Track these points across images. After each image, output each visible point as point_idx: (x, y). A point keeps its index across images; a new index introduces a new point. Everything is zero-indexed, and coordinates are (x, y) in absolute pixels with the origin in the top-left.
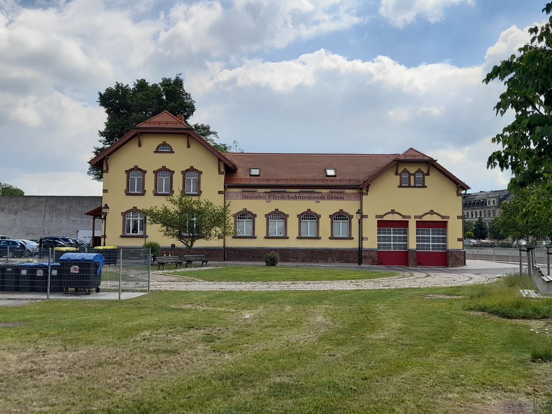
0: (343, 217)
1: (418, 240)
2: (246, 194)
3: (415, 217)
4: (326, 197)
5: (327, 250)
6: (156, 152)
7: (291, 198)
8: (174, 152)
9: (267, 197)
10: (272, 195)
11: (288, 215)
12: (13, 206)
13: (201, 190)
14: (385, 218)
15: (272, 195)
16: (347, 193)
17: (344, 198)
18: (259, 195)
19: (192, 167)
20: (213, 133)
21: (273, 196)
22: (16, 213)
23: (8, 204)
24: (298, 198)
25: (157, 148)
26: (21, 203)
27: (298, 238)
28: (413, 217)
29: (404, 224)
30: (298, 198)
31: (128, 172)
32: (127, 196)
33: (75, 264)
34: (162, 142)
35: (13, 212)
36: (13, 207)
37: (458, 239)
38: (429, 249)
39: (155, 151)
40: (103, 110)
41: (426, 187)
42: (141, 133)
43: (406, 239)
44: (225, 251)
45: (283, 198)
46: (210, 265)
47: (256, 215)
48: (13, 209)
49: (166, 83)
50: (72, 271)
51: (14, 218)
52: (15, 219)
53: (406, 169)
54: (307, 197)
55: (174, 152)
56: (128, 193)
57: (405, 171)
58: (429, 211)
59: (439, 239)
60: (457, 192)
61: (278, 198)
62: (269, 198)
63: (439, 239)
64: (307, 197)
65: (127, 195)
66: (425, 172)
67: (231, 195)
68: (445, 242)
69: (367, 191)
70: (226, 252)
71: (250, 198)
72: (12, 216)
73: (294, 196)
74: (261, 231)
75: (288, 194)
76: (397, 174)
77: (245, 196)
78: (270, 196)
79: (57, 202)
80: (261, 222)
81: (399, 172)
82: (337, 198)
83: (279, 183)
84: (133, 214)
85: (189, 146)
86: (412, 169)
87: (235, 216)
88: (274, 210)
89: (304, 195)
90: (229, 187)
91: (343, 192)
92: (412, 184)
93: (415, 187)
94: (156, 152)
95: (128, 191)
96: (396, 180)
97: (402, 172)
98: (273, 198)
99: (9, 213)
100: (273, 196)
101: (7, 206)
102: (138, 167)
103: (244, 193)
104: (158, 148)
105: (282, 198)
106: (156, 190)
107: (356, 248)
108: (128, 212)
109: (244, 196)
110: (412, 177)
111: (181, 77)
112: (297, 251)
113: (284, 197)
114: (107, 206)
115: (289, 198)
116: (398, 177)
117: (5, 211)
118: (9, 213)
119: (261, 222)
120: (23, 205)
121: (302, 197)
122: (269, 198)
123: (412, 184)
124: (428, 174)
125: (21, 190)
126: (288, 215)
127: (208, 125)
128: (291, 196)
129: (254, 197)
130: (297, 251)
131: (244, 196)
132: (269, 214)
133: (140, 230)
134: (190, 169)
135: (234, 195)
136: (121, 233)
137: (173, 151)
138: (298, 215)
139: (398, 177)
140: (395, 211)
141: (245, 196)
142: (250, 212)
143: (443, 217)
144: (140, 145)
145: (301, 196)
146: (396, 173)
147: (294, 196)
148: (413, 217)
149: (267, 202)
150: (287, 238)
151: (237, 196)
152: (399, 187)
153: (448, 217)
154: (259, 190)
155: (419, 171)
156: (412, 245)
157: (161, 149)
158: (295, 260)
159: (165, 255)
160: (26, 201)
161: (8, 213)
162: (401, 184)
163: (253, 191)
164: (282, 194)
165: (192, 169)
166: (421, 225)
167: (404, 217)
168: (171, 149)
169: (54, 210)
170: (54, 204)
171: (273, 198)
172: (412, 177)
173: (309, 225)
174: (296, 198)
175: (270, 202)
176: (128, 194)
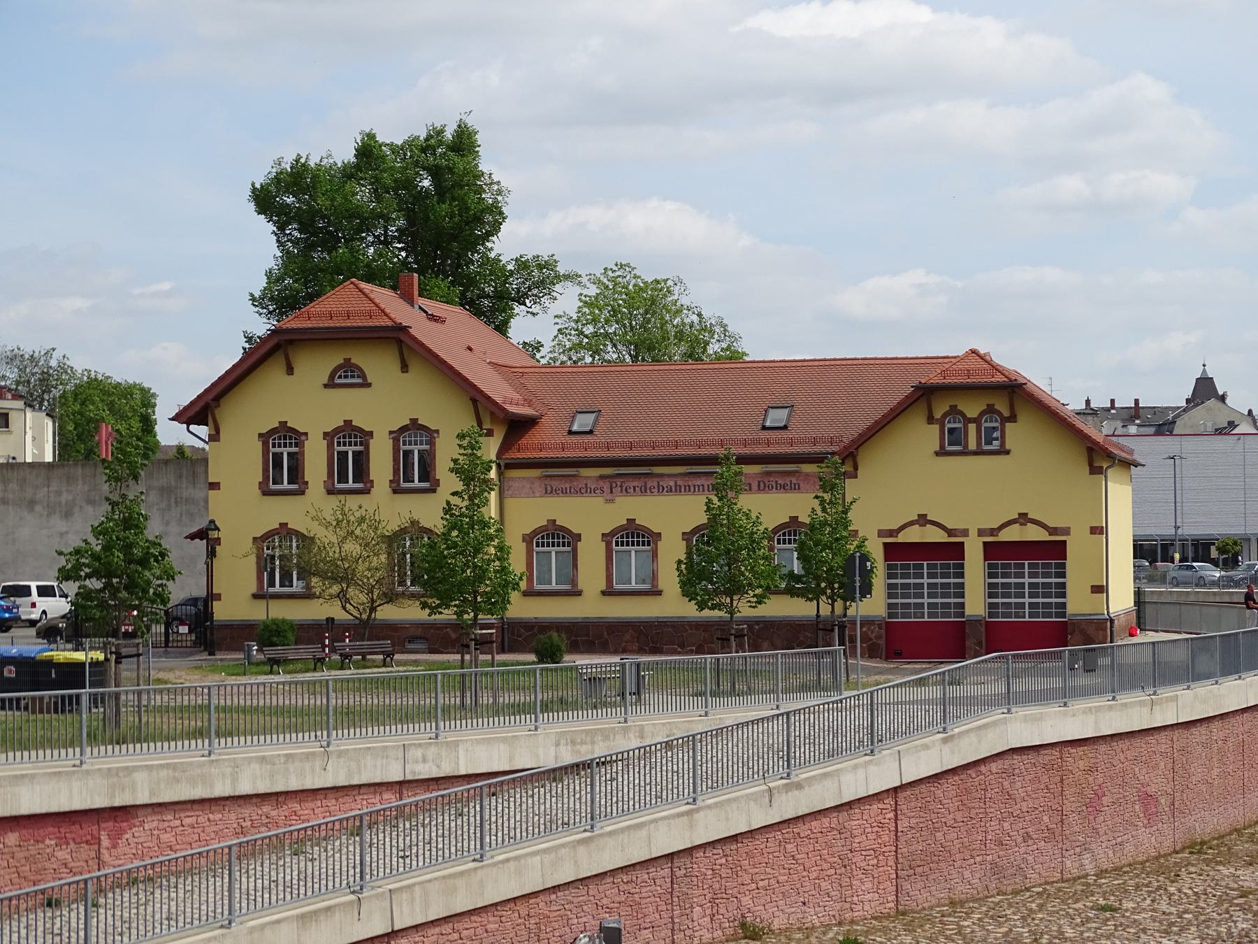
0: (638, 537)
1: (992, 591)
2: (555, 484)
3: (981, 532)
4: (755, 486)
5: (758, 623)
6: (330, 385)
7: (666, 489)
8: (369, 385)
9: (607, 489)
10: (619, 484)
11: (660, 533)
12: (59, 493)
13: (437, 478)
14: (901, 538)
15: (619, 484)
16: (807, 475)
17: (801, 485)
18: (586, 485)
19: (414, 421)
20: (567, 277)
21: (621, 486)
22: (68, 515)
23: (46, 489)
24: (683, 490)
25: (332, 373)
26: (80, 482)
27: (604, 593)
28: (973, 533)
29: (955, 551)
30: (683, 490)
31: (264, 437)
32: (265, 497)
33: (10, 664)
34: (342, 361)
35: (61, 511)
36: (60, 495)
37: (1092, 586)
38: (1021, 614)
39: (326, 382)
40: (264, 228)
41: (1008, 452)
42: (291, 342)
43: (960, 591)
44: (503, 629)
45: (646, 491)
46: (399, 663)
47: (579, 535)
48: (60, 503)
49: (432, 141)
50: (6, 674)
51: (64, 529)
52: (67, 533)
53: (956, 406)
54: (706, 487)
55: (369, 385)
56: (265, 489)
57: (954, 411)
58: (1017, 516)
59: (1006, 590)
60: (1091, 465)
61: (632, 490)
62: (611, 492)
63: (1006, 590)
64: (706, 487)
65: (264, 495)
66: (1006, 413)
67: (516, 485)
68: (1063, 595)
69: (856, 468)
70: (506, 632)
71: (564, 492)
72: (59, 524)
73: (672, 483)
74: (591, 573)
75: (658, 480)
76: (930, 420)
77: (552, 488)
78: (614, 485)
79: (180, 477)
80: (591, 555)
81: (938, 415)
82: (783, 488)
83: (635, 453)
84: (280, 541)
85: (405, 368)
86: (972, 409)
87: (528, 539)
88: (625, 522)
89: (699, 483)
90: (510, 466)
91: (796, 472)
92: (972, 445)
93: (979, 453)
94: (330, 385)
95: (268, 484)
96: (930, 436)
97: (945, 416)
98: (622, 492)
99: (48, 515)
100: (621, 486)
101: (42, 493)
102: (288, 425)
103: (548, 482)
104: (332, 377)
105: (644, 491)
106: (331, 481)
107: (810, 617)
108: (268, 535)
109: (549, 489)
110: (972, 428)
111: (470, 122)
112: (683, 626)
113: (648, 487)
114: (215, 525)
115: (661, 490)
116: (936, 428)
117: (38, 508)
118: (49, 515)
119: (591, 555)
120: (86, 488)
121: (694, 486)
122: (611, 492)
123: (972, 445)
124: (1013, 418)
125: (146, 385)
126: (660, 533)
127: (553, 255)
128: (665, 486)
129: (572, 490)
130: (683, 626)
131: (549, 489)
132: (613, 533)
133: (298, 579)
134: (410, 426)
135: (523, 487)
136: (253, 588)
137: (369, 381)
138: (684, 533)
139: (936, 428)
140: (928, 518)
141: (552, 488)
142: (563, 528)
143: (1053, 531)
144: (290, 370)
145: (690, 483)
146: (928, 418)
147: (672, 483)
148: (973, 533)
149: (608, 501)
150: (659, 593)
151: (531, 488)
152: (937, 454)
153: (1066, 531)
154: (585, 472)
155: (990, 410)
156: (975, 604)
157: (340, 377)
158: (679, 650)
159: (347, 640)
160: (95, 475)
161: (46, 513)
162: (942, 446)
163: (569, 476)
164: (642, 479)
165: (414, 426)
166: (994, 551)
167: (951, 532)
168: (363, 376)
169: (173, 500)
170: (173, 483)
171: (622, 492)
172: (972, 428)
173: (634, 557)
174: (677, 490)
175: (612, 501)
176: (266, 492)
